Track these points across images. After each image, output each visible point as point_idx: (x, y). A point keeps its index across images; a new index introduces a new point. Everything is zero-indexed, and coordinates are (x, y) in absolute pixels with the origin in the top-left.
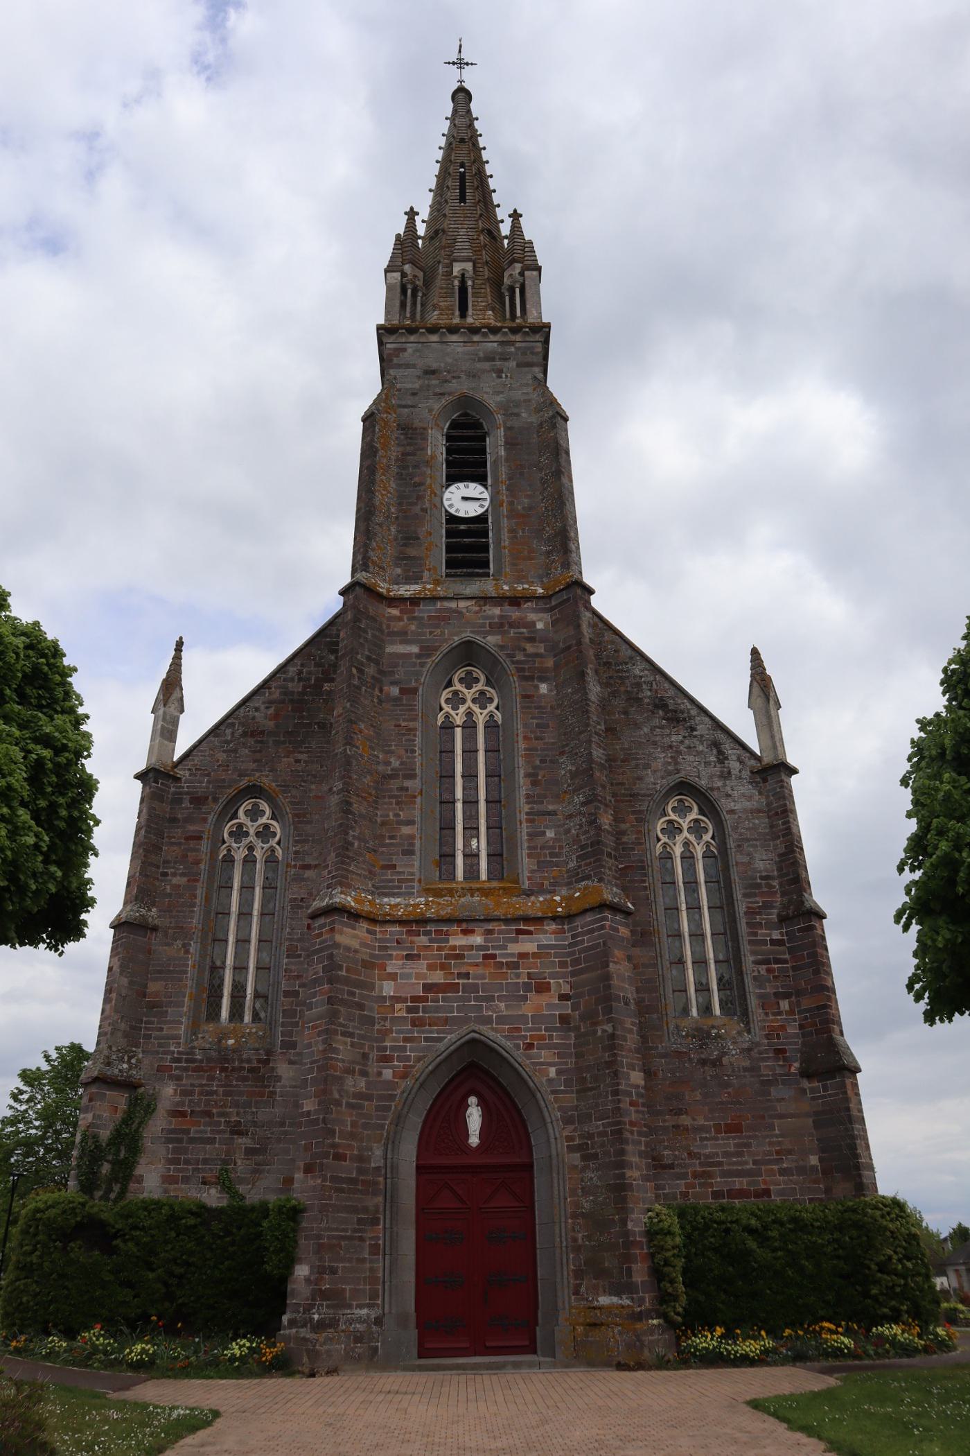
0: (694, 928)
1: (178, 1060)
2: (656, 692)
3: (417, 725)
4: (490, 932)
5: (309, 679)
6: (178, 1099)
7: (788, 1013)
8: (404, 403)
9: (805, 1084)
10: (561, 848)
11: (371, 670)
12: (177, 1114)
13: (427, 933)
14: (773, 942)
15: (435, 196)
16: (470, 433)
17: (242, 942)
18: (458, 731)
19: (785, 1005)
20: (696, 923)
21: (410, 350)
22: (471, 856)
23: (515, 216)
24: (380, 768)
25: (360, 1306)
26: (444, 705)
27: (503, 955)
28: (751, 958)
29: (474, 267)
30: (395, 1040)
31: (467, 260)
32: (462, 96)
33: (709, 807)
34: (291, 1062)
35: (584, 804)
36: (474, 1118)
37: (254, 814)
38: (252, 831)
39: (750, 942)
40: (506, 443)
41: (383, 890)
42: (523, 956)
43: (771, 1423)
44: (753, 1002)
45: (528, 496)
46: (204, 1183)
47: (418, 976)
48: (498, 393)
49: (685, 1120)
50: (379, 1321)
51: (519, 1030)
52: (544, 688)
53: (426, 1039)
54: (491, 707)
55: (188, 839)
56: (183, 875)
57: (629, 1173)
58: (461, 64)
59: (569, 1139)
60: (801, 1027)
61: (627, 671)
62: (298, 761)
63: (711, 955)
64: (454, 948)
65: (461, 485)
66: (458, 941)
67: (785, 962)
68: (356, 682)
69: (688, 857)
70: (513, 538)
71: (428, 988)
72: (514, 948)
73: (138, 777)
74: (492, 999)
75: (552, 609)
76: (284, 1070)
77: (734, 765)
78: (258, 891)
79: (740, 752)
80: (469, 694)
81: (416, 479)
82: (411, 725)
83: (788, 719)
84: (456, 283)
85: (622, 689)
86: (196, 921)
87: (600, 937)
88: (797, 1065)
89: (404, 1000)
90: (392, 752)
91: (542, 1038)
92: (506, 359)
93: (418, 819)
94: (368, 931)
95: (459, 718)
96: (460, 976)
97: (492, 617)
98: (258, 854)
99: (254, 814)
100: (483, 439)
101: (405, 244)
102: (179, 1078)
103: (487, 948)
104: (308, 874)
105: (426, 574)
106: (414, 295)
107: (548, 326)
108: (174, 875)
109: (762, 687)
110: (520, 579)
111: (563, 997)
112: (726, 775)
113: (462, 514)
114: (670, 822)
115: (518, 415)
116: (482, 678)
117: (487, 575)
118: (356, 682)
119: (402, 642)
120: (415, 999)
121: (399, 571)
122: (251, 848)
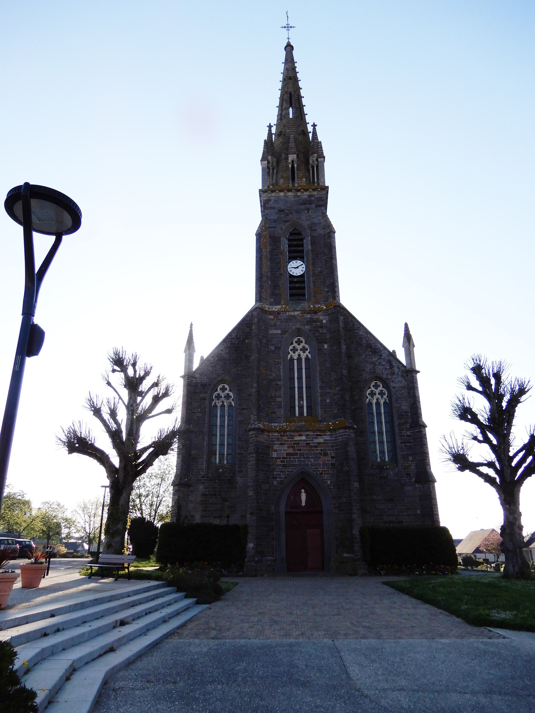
0: (379, 428)
1: (203, 477)
2: (368, 341)
3: (281, 361)
4: (307, 435)
5: (240, 338)
6: (204, 490)
7: (412, 461)
8: (271, 226)
9: (417, 485)
10: (332, 405)
11: (264, 341)
12: (204, 495)
13: (287, 436)
14: (408, 436)
15: (279, 110)
16: (297, 237)
17: (222, 435)
18: (295, 361)
19: (411, 458)
20: (380, 428)
21: (272, 201)
22: (301, 407)
23: (314, 126)
24: (269, 377)
25: (269, 556)
26: (290, 352)
27: (313, 443)
28: (400, 441)
29: (297, 156)
30: (277, 472)
31: (295, 154)
32: (289, 48)
33: (386, 386)
34: (241, 477)
35: (339, 391)
36: (303, 496)
37: (223, 389)
38: (223, 396)
39: (399, 436)
40: (311, 243)
41: (271, 421)
42: (319, 443)
43: (386, 587)
44: (399, 457)
45: (320, 267)
46: (215, 517)
47: (284, 450)
48: (307, 220)
49: (374, 497)
50: (275, 561)
51: (318, 468)
52: (326, 346)
53: (288, 471)
54: (307, 352)
55: (201, 399)
56: (200, 413)
57: (353, 516)
58: (288, 27)
59: (335, 504)
60: (416, 466)
61: (357, 333)
62: (238, 370)
63: (385, 440)
64: (296, 441)
65: (294, 261)
66: (297, 438)
67: (412, 443)
68: (259, 347)
69: (378, 404)
70: (314, 285)
71: (287, 454)
72: (316, 441)
73: (181, 377)
74: (309, 458)
75: (328, 315)
76: (239, 480)
77: (396, 370)
78: (226, 417)
79: (399, 364)
80: (299, 347)
81: (278, 261)
82: (279, 361)
83: (417, 351)
84: (290, 166)
85: (355, 340)
86: (206, 429)
87: (345, 438)
88: (414, 479)
89: (280, 458)
90: (272, 371)
91: (326, 471)
92: (310, 204)
93: (282, 396)
94: (267, 435)
95: (295, 356)
96: (298, 450)
97: (307, 318)
98: (225, 404)
99: (223, 389)
100: (302, 240)
101: (268, 144)
102: (204, 483)
103: (307, 441)
104: (244, 411)
105: (282, 301)
106: (273, 169)
107: (328, 187)
108: (197, 413)
109: (408, 338)
110: (318, 303)
111: (332, 457)
112: (393, 374)
113: (295, 274)
114: (372, 391)
115: (316, 230)
116: (304, 341)
117: (305, 300)
118: (259, 347)
119: (275, 329)
120: (283, 458)
121: (272, 300)
122: (223, 402)
